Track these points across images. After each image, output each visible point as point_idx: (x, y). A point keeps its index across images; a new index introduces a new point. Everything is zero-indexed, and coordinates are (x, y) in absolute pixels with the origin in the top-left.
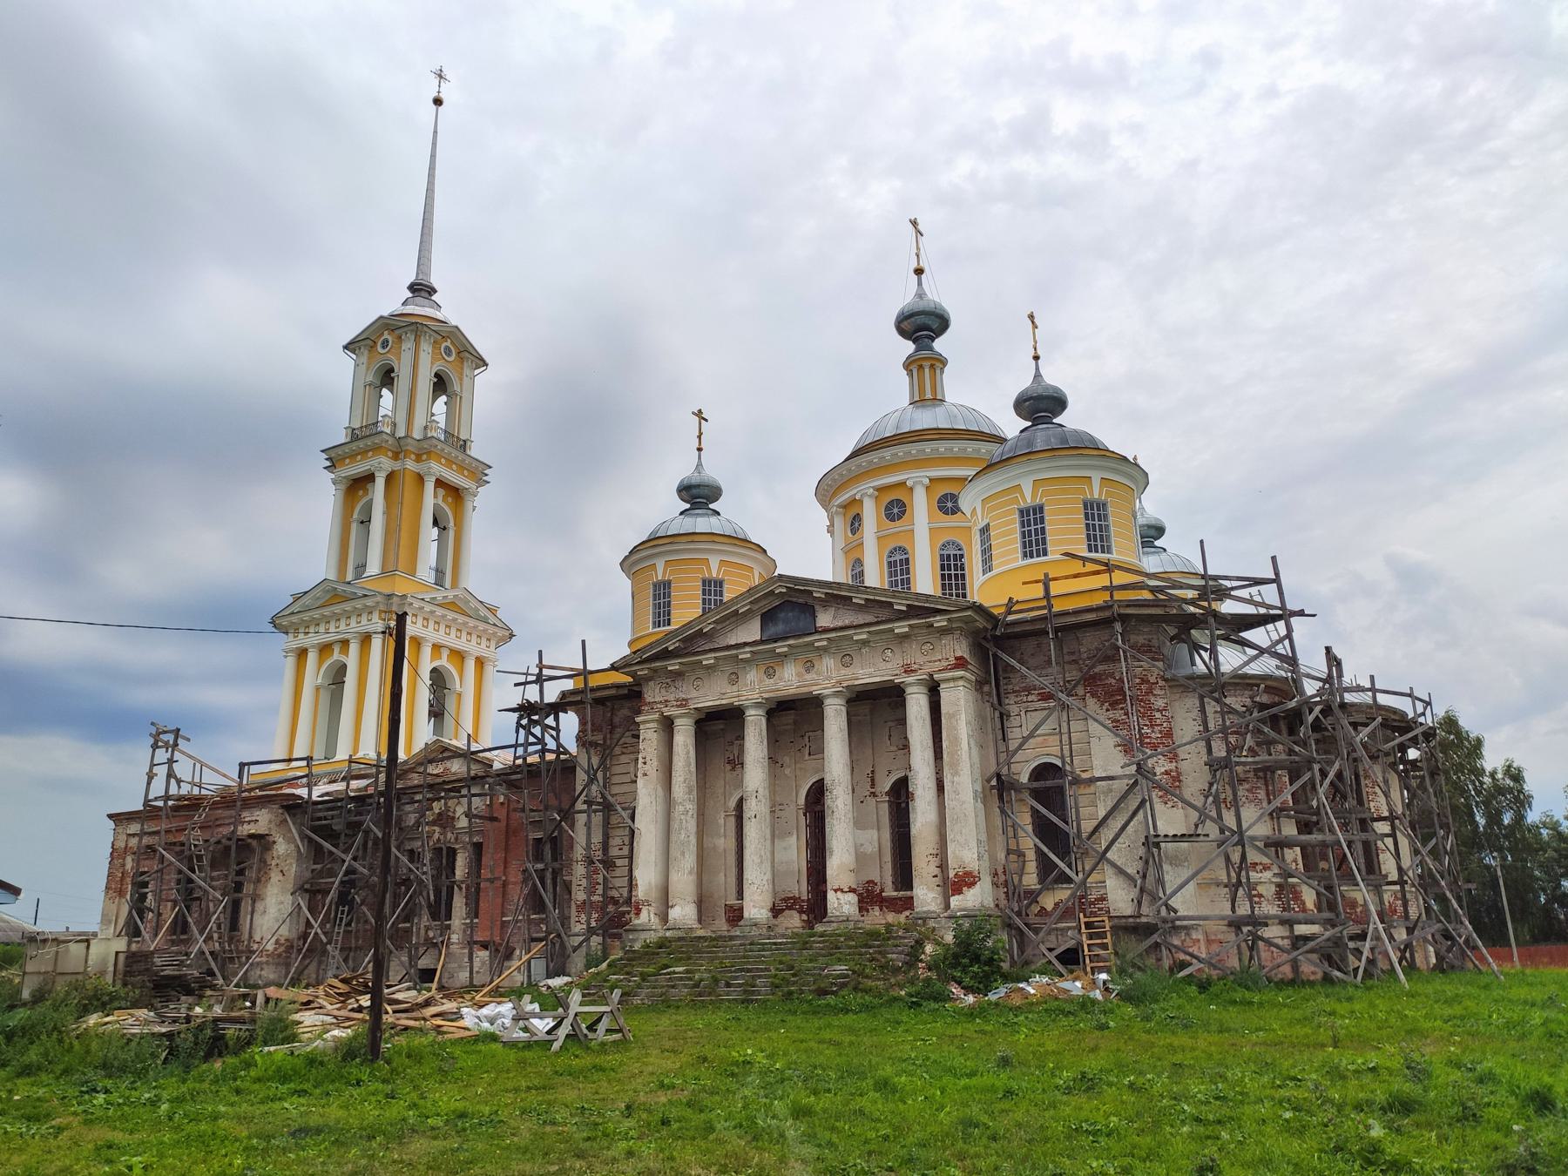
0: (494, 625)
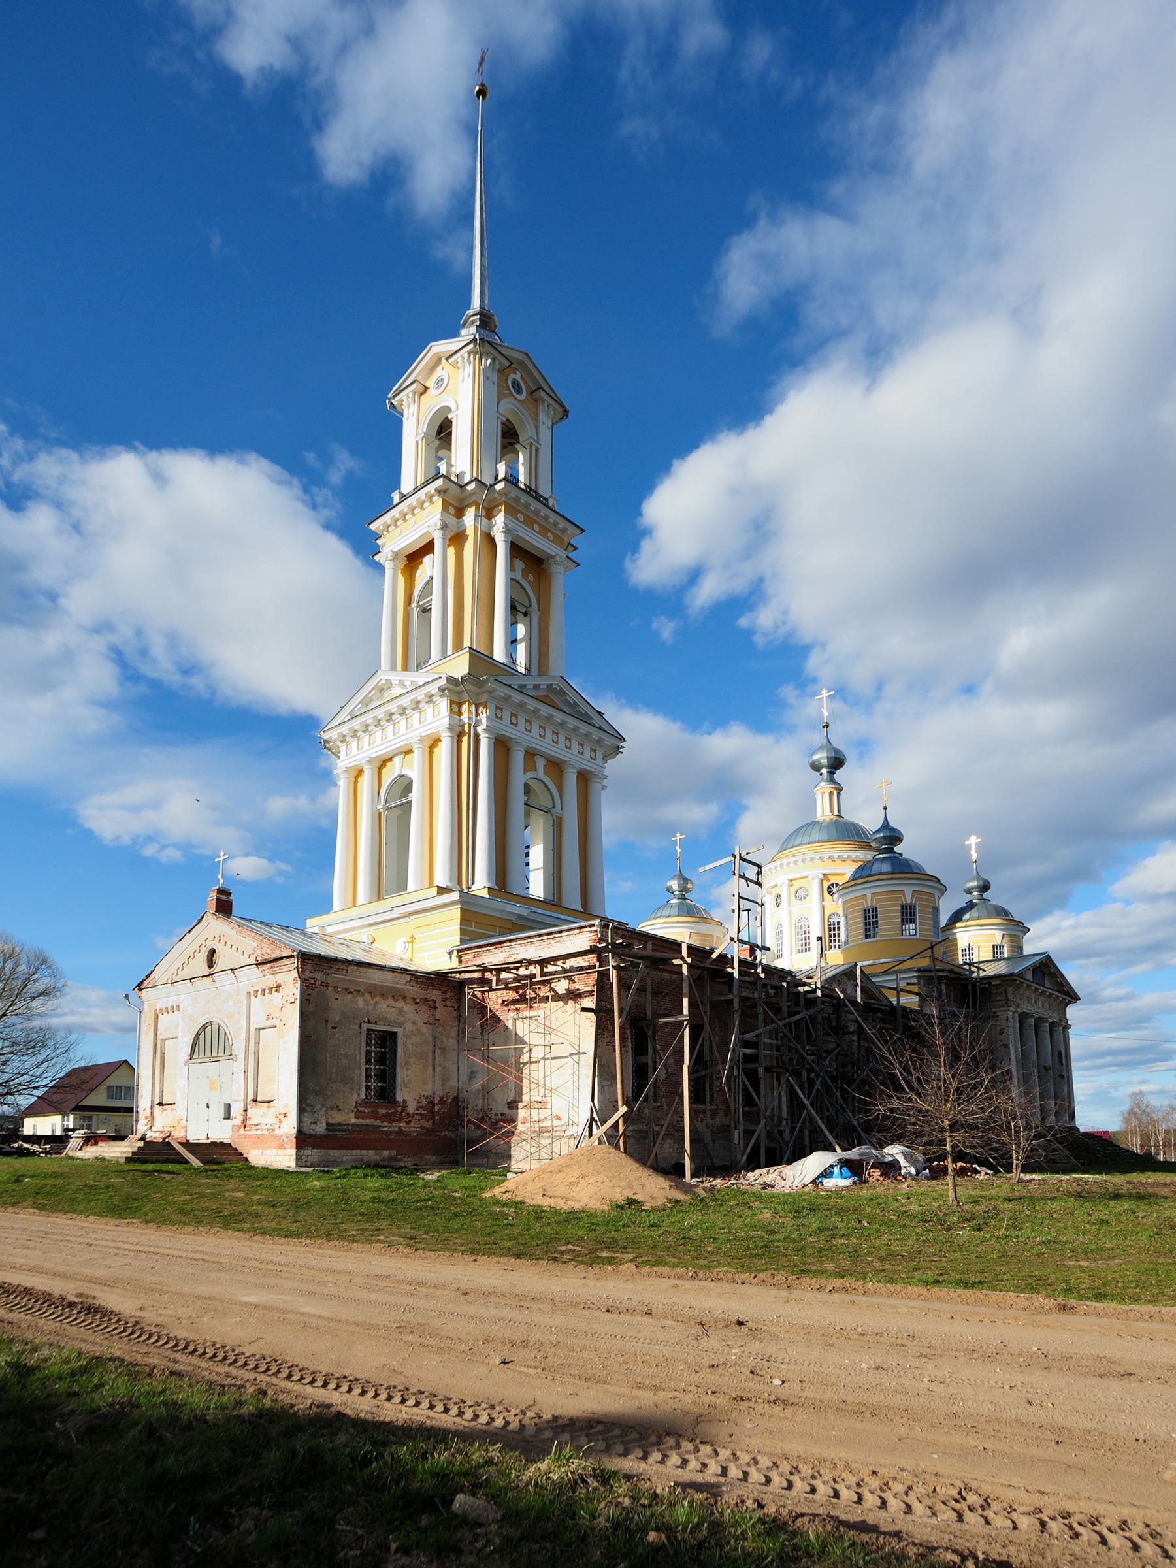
0: (600, 728)
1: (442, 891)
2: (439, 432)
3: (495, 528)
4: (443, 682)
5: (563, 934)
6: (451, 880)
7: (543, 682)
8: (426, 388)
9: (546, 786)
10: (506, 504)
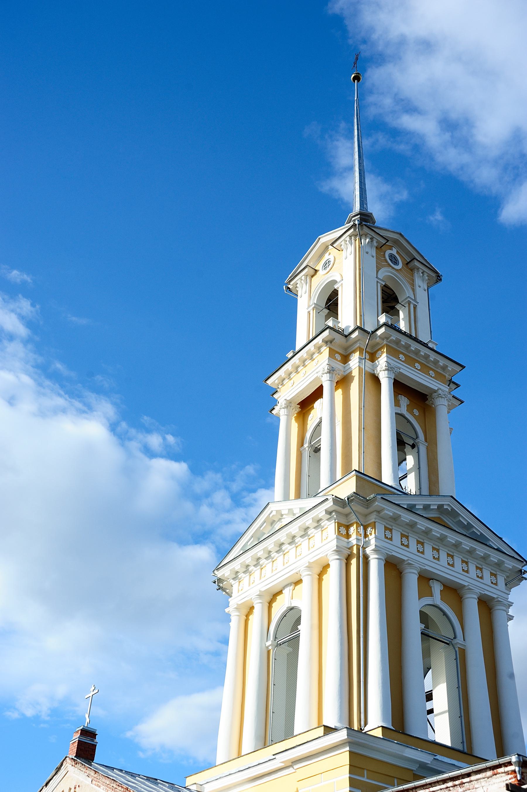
1: (328, 730)
2: (329, 300)
3: (379, 369)
4: (329, 504)
5: (473, 778)
6: (340, 720)
7: (434, 503)
8: (316, 271)
9: (445, 614)
10: (388, 346)
